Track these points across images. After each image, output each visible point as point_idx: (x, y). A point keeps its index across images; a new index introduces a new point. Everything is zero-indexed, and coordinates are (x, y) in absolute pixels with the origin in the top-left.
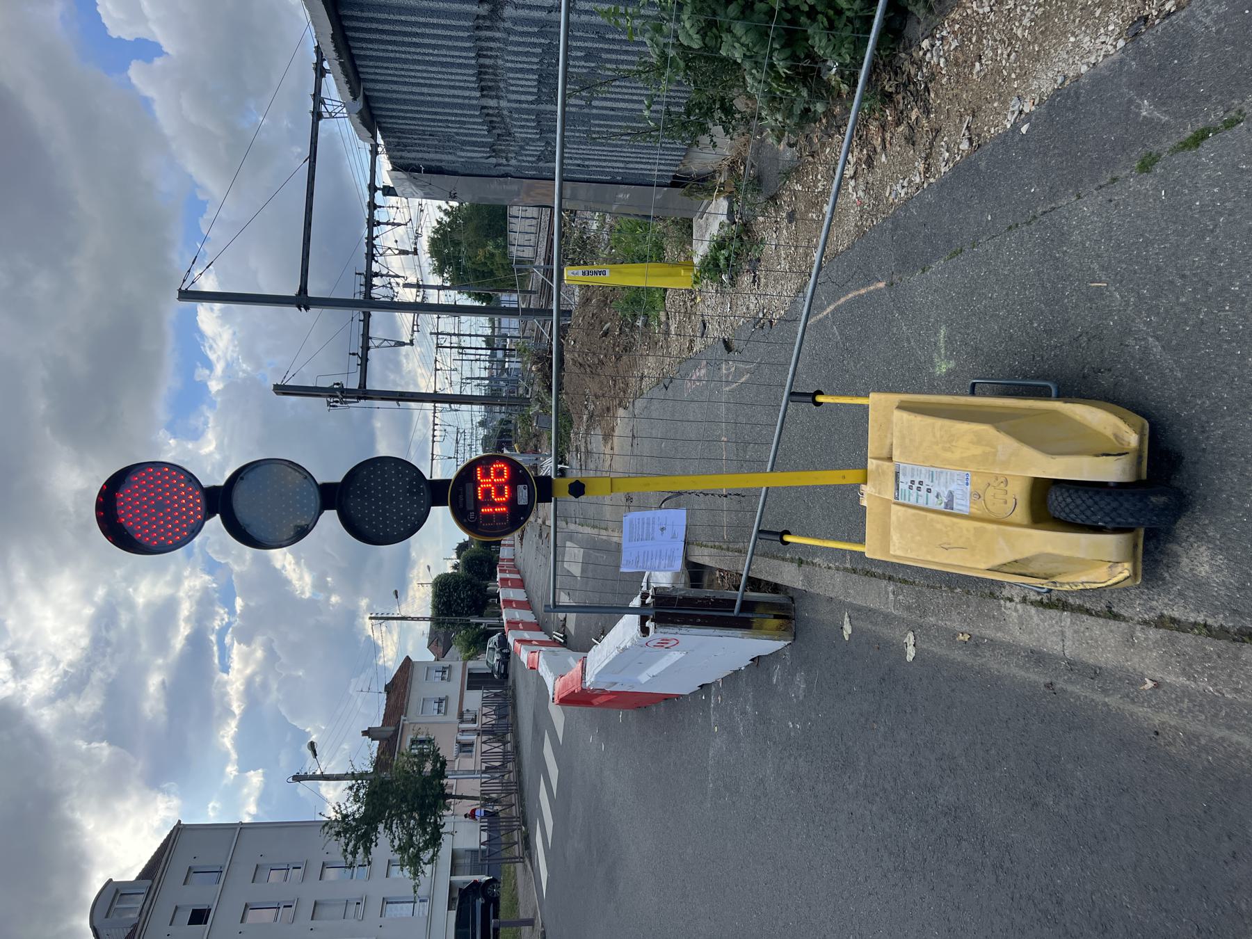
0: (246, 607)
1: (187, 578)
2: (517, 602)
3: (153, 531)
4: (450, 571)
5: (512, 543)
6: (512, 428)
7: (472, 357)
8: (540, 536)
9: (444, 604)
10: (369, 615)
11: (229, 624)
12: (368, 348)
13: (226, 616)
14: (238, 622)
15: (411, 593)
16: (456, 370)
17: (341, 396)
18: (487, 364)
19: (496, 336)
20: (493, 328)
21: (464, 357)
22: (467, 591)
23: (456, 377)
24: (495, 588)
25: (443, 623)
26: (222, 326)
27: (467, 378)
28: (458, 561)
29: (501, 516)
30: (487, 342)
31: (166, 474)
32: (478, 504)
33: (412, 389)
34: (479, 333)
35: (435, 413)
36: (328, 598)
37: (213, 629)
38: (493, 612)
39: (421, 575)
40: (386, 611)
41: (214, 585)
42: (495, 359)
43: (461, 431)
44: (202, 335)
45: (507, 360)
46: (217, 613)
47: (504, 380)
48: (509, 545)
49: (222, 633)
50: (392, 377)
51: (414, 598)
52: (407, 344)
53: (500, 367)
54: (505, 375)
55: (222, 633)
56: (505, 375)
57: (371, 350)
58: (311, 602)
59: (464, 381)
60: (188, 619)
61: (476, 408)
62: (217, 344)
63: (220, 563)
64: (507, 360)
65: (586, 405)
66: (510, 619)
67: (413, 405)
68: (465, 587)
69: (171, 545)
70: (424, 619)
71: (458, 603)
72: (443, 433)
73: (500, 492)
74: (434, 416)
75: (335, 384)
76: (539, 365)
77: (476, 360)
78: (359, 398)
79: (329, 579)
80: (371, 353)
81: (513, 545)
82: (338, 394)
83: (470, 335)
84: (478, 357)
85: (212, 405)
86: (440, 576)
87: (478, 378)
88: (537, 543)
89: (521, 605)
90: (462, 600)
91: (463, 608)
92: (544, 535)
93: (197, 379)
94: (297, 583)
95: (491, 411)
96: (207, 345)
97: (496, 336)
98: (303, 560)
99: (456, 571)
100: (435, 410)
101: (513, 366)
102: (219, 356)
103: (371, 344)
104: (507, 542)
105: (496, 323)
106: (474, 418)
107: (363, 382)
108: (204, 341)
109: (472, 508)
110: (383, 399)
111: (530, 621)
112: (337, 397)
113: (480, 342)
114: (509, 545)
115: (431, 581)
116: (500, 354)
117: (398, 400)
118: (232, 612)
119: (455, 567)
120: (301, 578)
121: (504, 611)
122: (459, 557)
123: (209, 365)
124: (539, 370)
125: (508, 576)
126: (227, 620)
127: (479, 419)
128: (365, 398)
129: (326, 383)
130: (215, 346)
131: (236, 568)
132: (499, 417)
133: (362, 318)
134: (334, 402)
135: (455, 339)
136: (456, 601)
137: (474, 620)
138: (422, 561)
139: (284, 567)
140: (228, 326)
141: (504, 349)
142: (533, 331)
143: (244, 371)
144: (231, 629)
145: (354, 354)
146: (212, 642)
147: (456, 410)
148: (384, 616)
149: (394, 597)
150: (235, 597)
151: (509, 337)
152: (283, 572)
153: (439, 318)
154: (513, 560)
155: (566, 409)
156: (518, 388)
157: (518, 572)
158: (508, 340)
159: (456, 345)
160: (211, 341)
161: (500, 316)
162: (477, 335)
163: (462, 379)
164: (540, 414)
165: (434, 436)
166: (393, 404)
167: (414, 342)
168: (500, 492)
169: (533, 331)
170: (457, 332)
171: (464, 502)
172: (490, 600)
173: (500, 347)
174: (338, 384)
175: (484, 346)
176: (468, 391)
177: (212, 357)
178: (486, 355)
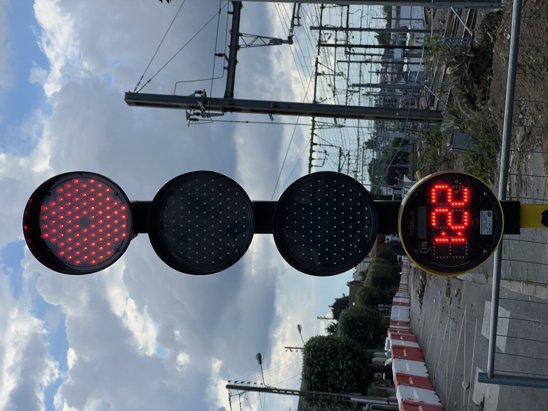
0: (80, 362)
1: (13, 320)
2: (415, 378)
3: (76, 249)
4: (325, 334)
5: (406, 301)
6: (410, 151)
7: (361, 58)
8: (448, 293)
9: (318, 375)
10: (227, 383)
11: (60, 381)
12: (238, 48)
13: (56, 371)
14: (69, 380)
15: (274, 358)
16: (342, 74)
17: (203, 108)
18: (380, 67)
19: (393, 30)
20: (389, 19)
21: (352, 58)
22: (347, 361)
23: (341, 84)
24: (382, 359)
25: (317, 399)
26: (62, 14)
27: (354, 85)
28: (335, 321)
29: (457, 247)
30: (380, 38)
31: (91, 186)
32: (433, 233)
33: (284, 98)
34: (372, 26)
35: (313, 129)
36: (174, 356)
37: (41, 386)
38: (379, 391)
39: (287, 336)
40: (245, 379)
41: (45, 331)
42: (390, 60)
43: (346, 153)
44: (39, 28)
45: (406, 61)
46: (47, 366)
47: (401, 88)
48: (403, 304)
49: (50, 392)
50: (259, 80)
51: (278, 365)
52: (285, 42)
53: (395, 71)
54: (403, 81)
55: (50, 392)
56: (403, 81)
57: (241, 49)
58: (155, 360)
59: (351, 89)
60: (12, 370)
61: (364, 123)
62: (55, 38)
63: (52, 305)
64: (406, 61)
65: (520, 119)
66: (406, 398)
67: (285, 118)
68: (345, 355)
69: (95, 265)
70: (293, 393)
71: (335, 375)
72: (323, 156)
73: (458, 219)
74: (313, 134)
75: (196, 92)
76: (456, 67)
77: (366, 62)
78: (225, 110)
79: (177, 332)
80: (240, 55)
81: (409, 305)
82: (200, 104)
83: (361, 30)
84: (368, 57)
85: (48, 110)
86: (313, 339)
87: (368, 85)
88: (442, 302)
89: (419, 382)
90: (341, 372)
91: (341, 382)
92: (454, 292)
93: (33, 81)
94: (138, 334)
95: (383, 127)
96: (44, 40)
97: (393, 30)
98: (146, 307)
99: (332, 334)
100: (313, 125)
101: (414, 68)
102: (57, 53)
103: (241, 42)
104: (400, 300)
105: (394, 13)
106: (361, 138)
107: (230, 90)
108: (41, 35)
109: (424, 236)
110: (253, 111)
111: (433, 403)
112: (198, 108)
113: (371, 38)
114: (403, 304)
115: (302, 346)
116: (398, 53)
117: (271, 113)
118: (63, 366)
119: (331, 329)
120: (144, 330)
121: (398, 388)
122: (336, 317)
123: (45, 64)
124: (455, 74)
125: (403, 343)
126: (57, 376)
127: (367, 138)
128: (232, 110)
129: (186, 91)
130: (53, 41)
131: (69, 312)
132: (394, 135)
133: (231, 9)
134: (195, 114)
135: (341, 35)
136: (332, 372)
137: (355, 399)
138: (289, 318)
139: (125, 314)
140: (69, 15)
141: (403, 46)
142: (444, 22)
143: (85, 70)
144: (61, 387)
145: (220, 55)
146: (40, 401)
147: (341, 126)
148: (245, 385)
149: (257, 362)
150: (67, 348)
151: (409, 31)
152: (124, 320)
153: (322, 7)
154: (408, 324)
155: (491, 125)
156: (418, 98)
157: (416, 340)
158: (408, 35)
159: (343, 43)
160: (49, 35)
161: (399, 4)
162: (369, 30)
163: (348, 86)
164: (456, 131)
165: (311, 159)
166: (265, 117)
167: (294, 39)
168: (458, 219)
169: (444, 22)
170: (344, 26)
171: (416, 229)
172: (376, 375)
173: (397, 44)
174: (200, 92)
175: (377, 43)
176: (355, 101)
177: (50, 54)
178: (379, 55)
